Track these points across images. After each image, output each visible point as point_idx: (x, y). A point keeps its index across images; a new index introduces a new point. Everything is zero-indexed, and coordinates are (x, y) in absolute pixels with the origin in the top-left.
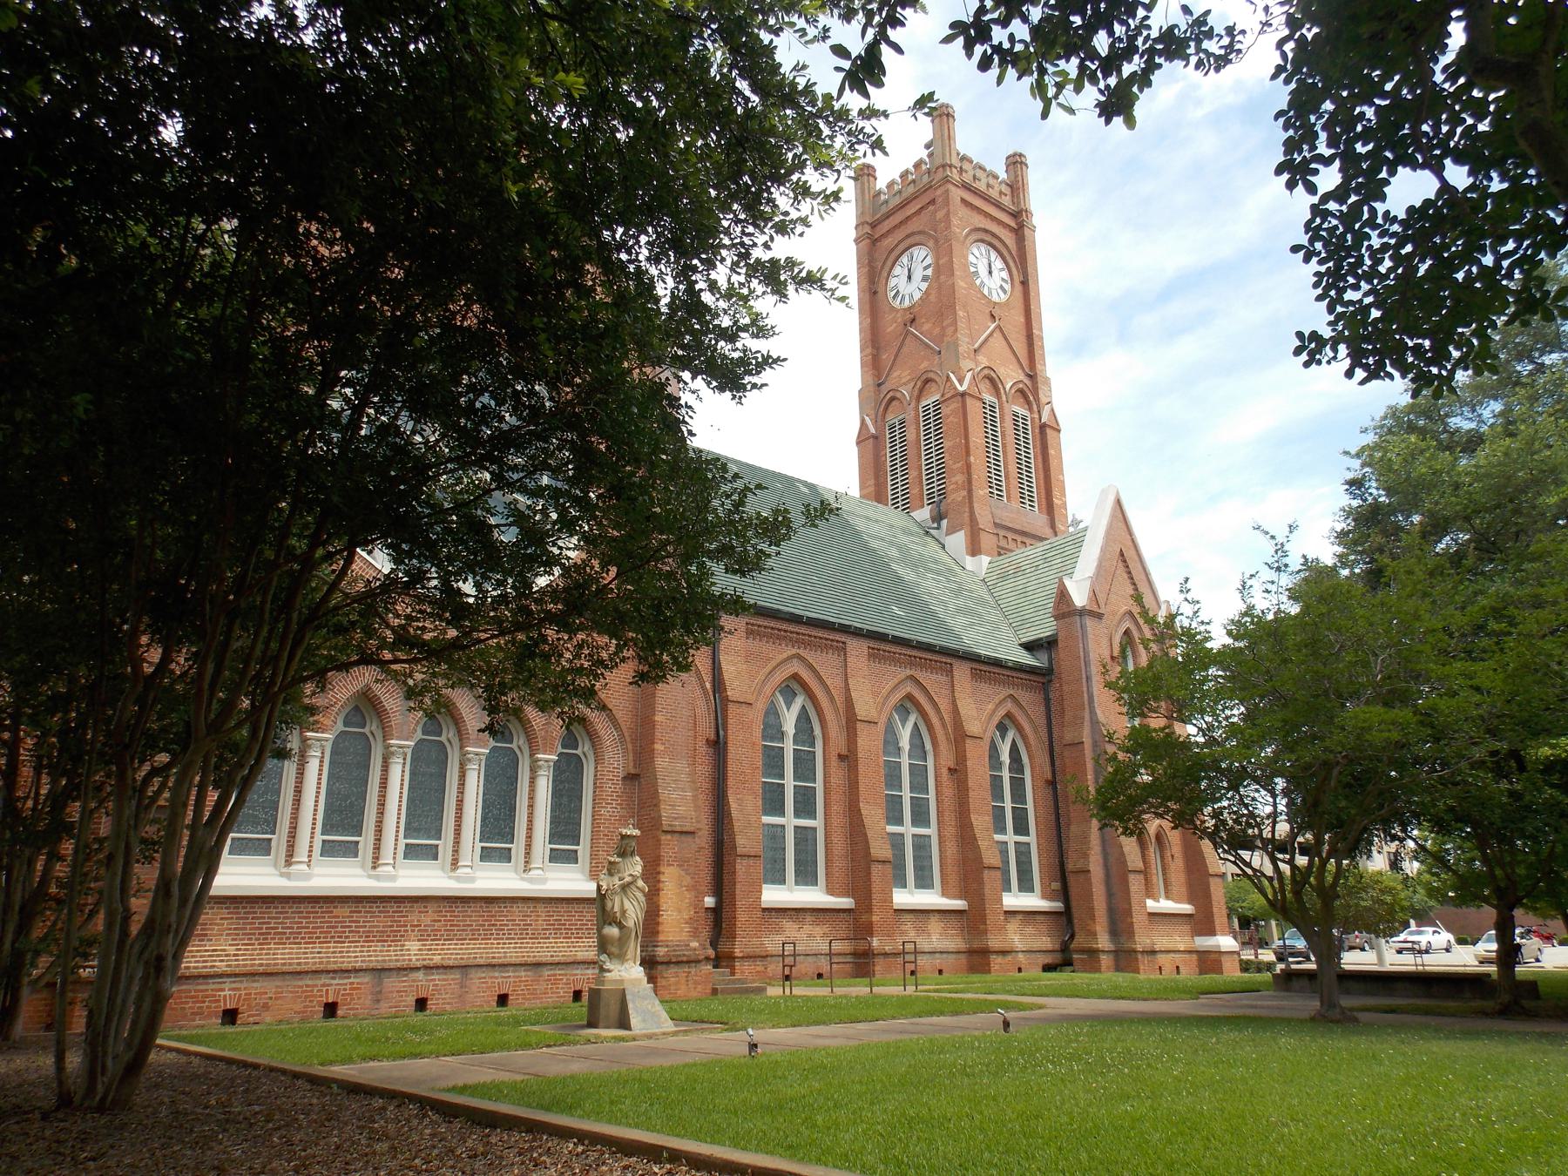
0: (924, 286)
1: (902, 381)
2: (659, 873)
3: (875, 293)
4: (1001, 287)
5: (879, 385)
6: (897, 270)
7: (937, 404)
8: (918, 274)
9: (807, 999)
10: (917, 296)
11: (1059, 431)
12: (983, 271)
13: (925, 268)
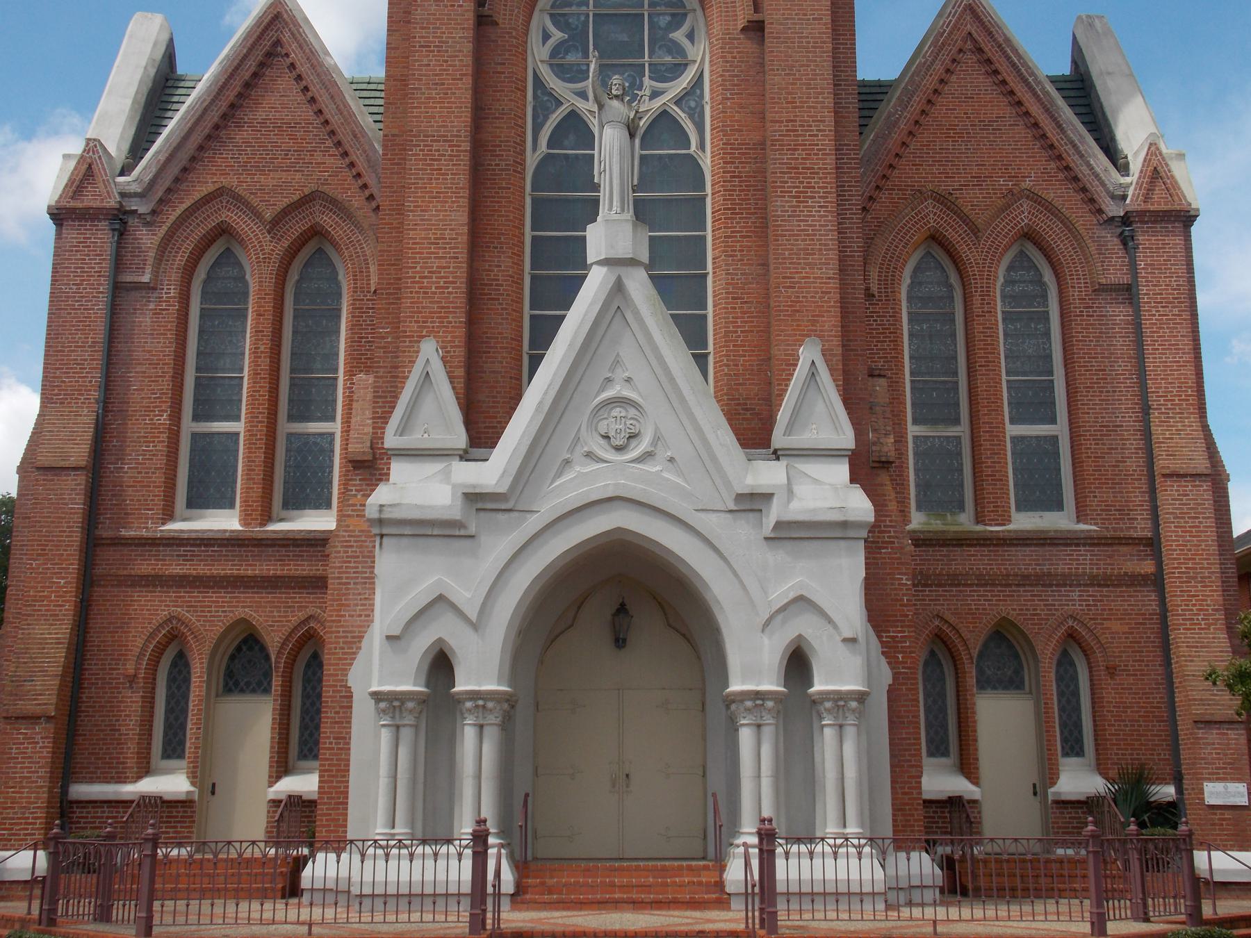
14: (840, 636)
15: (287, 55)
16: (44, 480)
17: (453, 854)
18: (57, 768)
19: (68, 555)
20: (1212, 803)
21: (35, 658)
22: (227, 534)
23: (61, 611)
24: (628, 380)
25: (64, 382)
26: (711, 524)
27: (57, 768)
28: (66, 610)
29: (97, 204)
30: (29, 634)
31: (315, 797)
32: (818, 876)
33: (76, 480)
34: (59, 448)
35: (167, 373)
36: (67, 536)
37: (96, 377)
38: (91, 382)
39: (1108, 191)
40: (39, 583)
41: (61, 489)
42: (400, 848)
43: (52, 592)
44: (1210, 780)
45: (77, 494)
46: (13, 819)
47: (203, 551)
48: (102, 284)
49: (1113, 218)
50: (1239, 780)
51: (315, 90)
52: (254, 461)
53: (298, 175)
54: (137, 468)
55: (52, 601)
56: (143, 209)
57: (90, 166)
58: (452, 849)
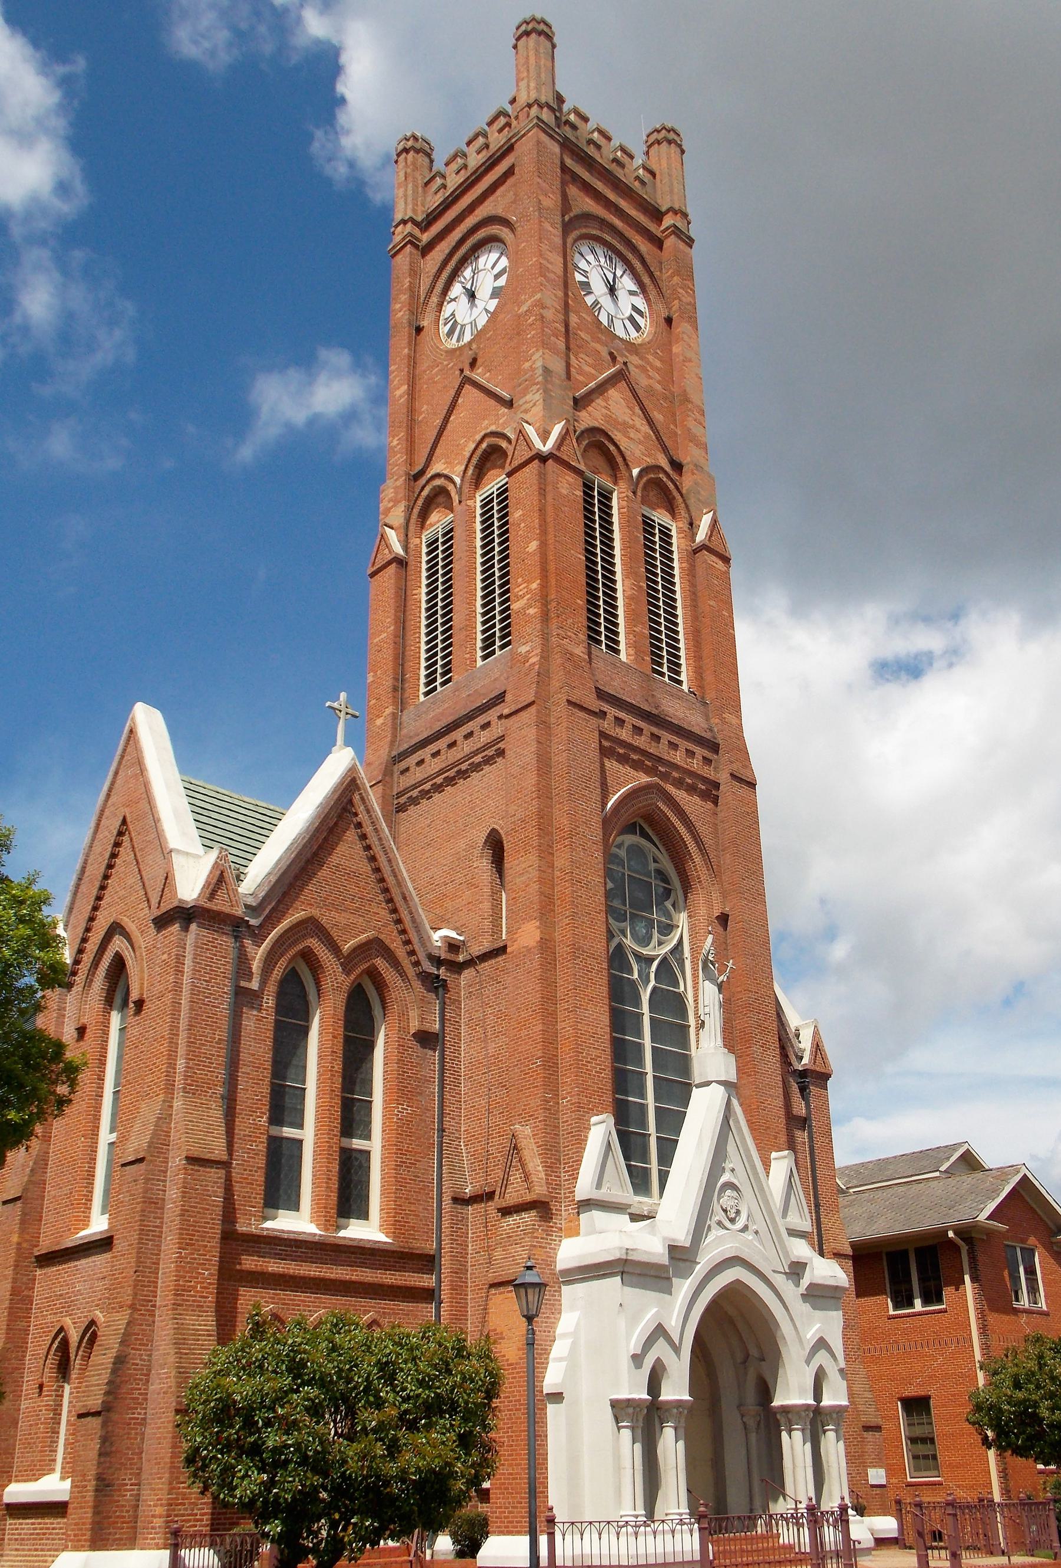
0: (492, 305)
1: (538, 1205)
2: (53, 988)
3: (419, 330)
4: (631, 319)
5: (417, 477)
6: (456, 290)
7: (503, 491)
8: (484, 292)
9: (580, 1143)
10: (482, 321)
11: (752, 785)
12: (599, 288)
13: (497, 277)
14: (837, 1366)
15: (356, 815)
16: (192, 1170)
17: (667, 1531)
18: (68, 1463)
19: (211, 1247)
20: (873, 1483)
21: (194, 1349)
22: (317, 1238)
23: (205, 1302)
24: (733, 1170)
25: (196, 1073)
26: (779, 1281)
27: (68, 1463)
28: (210, 1302)
29: (227, 910)
30: (183, 1324)
31: (65, 1497)
32: (641, 1551)
33: (217, 1173)
34: (201, 1139)
35: (267, 1077)
36: (211, 1228)
37: (221, 1074)
38: (217, 1077)
39: (794, 1052)
40: (187, 1272)
41: (206, 1181)
42: (682, 1525)
43: (198, 1283)
44: (870, 1467)
45: (218, 1187)
46: (183, 1515)
47: (294, 1252)
48: (226, 986)
49: (795, 1070)
50: (881, 1467)
51: (377, 849)
52: (331, 1171)
53: (361, 920)
54: (243, 1165)
55: (198, 1292)
56: (253, 922)
57: (222, 872)
58: (666, 1527)
